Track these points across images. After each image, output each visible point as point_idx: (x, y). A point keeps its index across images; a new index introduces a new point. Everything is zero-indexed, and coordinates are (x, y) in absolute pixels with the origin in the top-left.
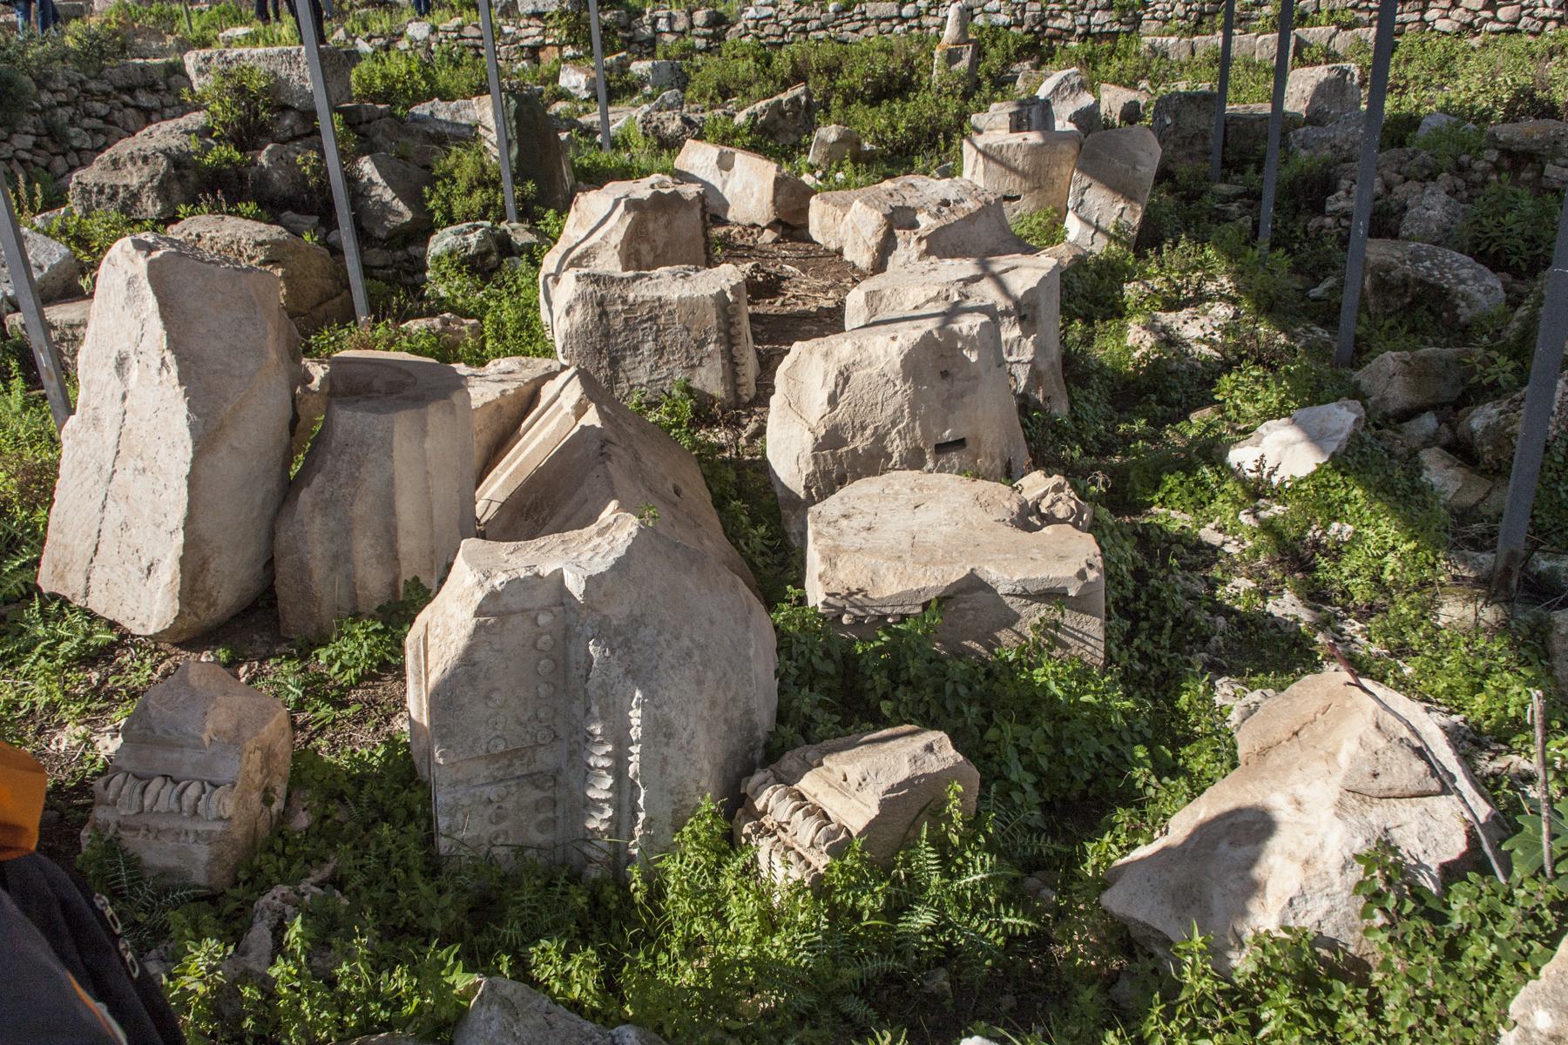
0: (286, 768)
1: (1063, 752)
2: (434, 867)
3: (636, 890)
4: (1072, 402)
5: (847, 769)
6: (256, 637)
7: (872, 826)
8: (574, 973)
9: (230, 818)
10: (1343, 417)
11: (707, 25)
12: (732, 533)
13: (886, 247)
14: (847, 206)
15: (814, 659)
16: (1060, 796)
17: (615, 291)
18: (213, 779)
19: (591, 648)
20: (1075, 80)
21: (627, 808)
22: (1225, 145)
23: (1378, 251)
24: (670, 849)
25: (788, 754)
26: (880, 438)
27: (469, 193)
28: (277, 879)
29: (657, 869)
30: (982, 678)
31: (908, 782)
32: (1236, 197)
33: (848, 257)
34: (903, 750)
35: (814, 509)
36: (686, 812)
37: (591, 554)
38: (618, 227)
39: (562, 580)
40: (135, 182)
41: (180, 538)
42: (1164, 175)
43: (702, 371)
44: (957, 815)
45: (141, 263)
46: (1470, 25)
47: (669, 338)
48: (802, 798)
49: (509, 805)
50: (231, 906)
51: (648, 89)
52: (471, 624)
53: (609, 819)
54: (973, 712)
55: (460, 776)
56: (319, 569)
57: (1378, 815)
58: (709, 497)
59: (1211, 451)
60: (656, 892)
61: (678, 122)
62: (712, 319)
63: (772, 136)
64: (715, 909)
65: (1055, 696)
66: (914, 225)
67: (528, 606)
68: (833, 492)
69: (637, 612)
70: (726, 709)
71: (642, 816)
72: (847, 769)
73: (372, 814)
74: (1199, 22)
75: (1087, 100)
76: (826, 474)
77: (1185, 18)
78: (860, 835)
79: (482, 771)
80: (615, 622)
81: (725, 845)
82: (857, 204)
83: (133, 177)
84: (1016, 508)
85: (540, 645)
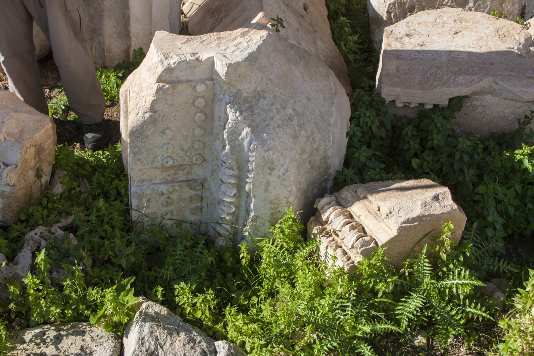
0: (51, 159)
1: (526, 205)
2: (128, 227)
3: (243, 258)
5: (381, 204)
6: (49, 74)
7: (391, 242)
8: (198, 305)
9: (14, 185)
12: (337, 37)
15: (373, 127)
16: (518, 232)
18: (5, 161)
19: (228, 110)
21: (243, 208)
24: (266, 235)
25: (346, 187)
28: (41, 222)
29: (258, 246)
30: (480, 151)
31: (419, 219)
34: (420, 197)
35: (388, 29)
36: (279, 215)
37: (234, 48)
39: (213, 64)
44: (448, 242)
48: (351, 217)
49: (174, 196)
50: (15, 234)
52: (155, 87)
53: (233, 213)
54: (470, 174)
55: (145, 177)
58: (325, 12)
60: (256, 260)
64: (289, 276)
65: (527, 169)
67: (191, 78)
68: (404, 17)
69: (259, 89)
70: (311, 154)
71: (252, 214)
72: (381, 204)
73: (98, 191)
78: (383, 246)
79: (159, 176)
80: (245, 94)
81: (300, 237)
84: (522, 41)
85: (197, 103)
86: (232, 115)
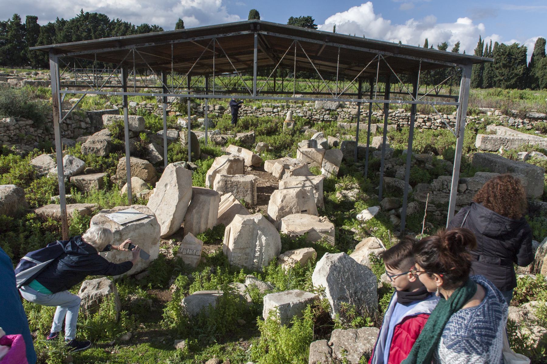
4: (325, 207)
7: (301, 259)
10: (376, 209)
11: (219, 110)
13: (283, 173)
14: (274, 163)
17: (229, 179)
20: (322, 135)
22: (358, 153)
23: (387, 179)
26: (291, 209)
27: (177, 154)
32: (361, 166)
33: (273, 175)
38: (227, 166)
40: (99, 147)
41: (172, 217)
42: (344, 160)
43: (246, 197)
45: (175, 168)
46: (420, 126)
47: (240, 190)
51: (203, 126)
56: (194, 224)
57: (372, 250)
59: (354, 216)
61: (221, 138)
62: (249, 186)
63: (245, 143)
66: (289, 169)
74: (352, 120)
75: (325, 140)
76: (280, 215)
77: (349, 118)
82: (276, 163)
83: (99, 146)
86: (259, 232)
